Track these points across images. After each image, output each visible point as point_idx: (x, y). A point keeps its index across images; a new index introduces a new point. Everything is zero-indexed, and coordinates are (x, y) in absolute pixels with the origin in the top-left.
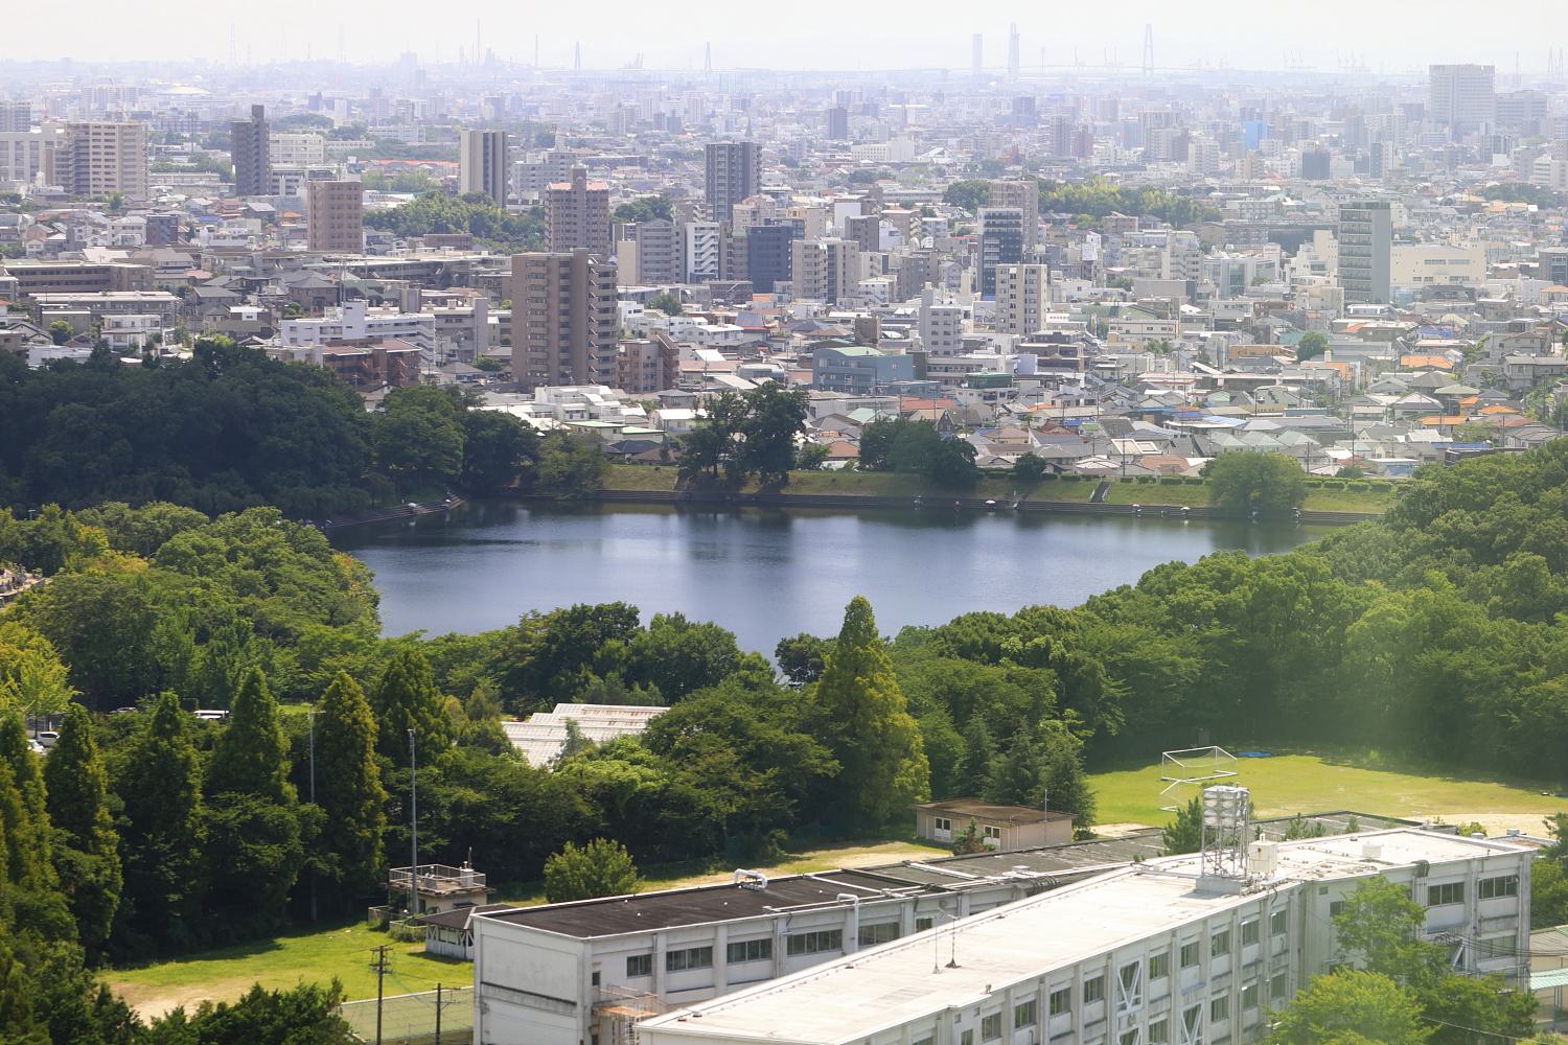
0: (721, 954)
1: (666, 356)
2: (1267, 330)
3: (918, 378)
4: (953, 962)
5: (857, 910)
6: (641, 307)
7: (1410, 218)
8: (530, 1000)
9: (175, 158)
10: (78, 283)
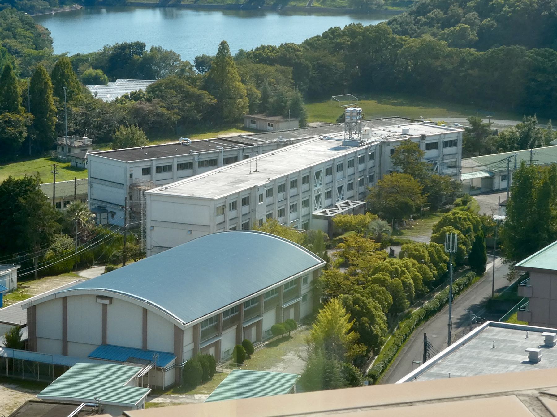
0: (175, 167)
5: (223, 152)
8: (108, 183)
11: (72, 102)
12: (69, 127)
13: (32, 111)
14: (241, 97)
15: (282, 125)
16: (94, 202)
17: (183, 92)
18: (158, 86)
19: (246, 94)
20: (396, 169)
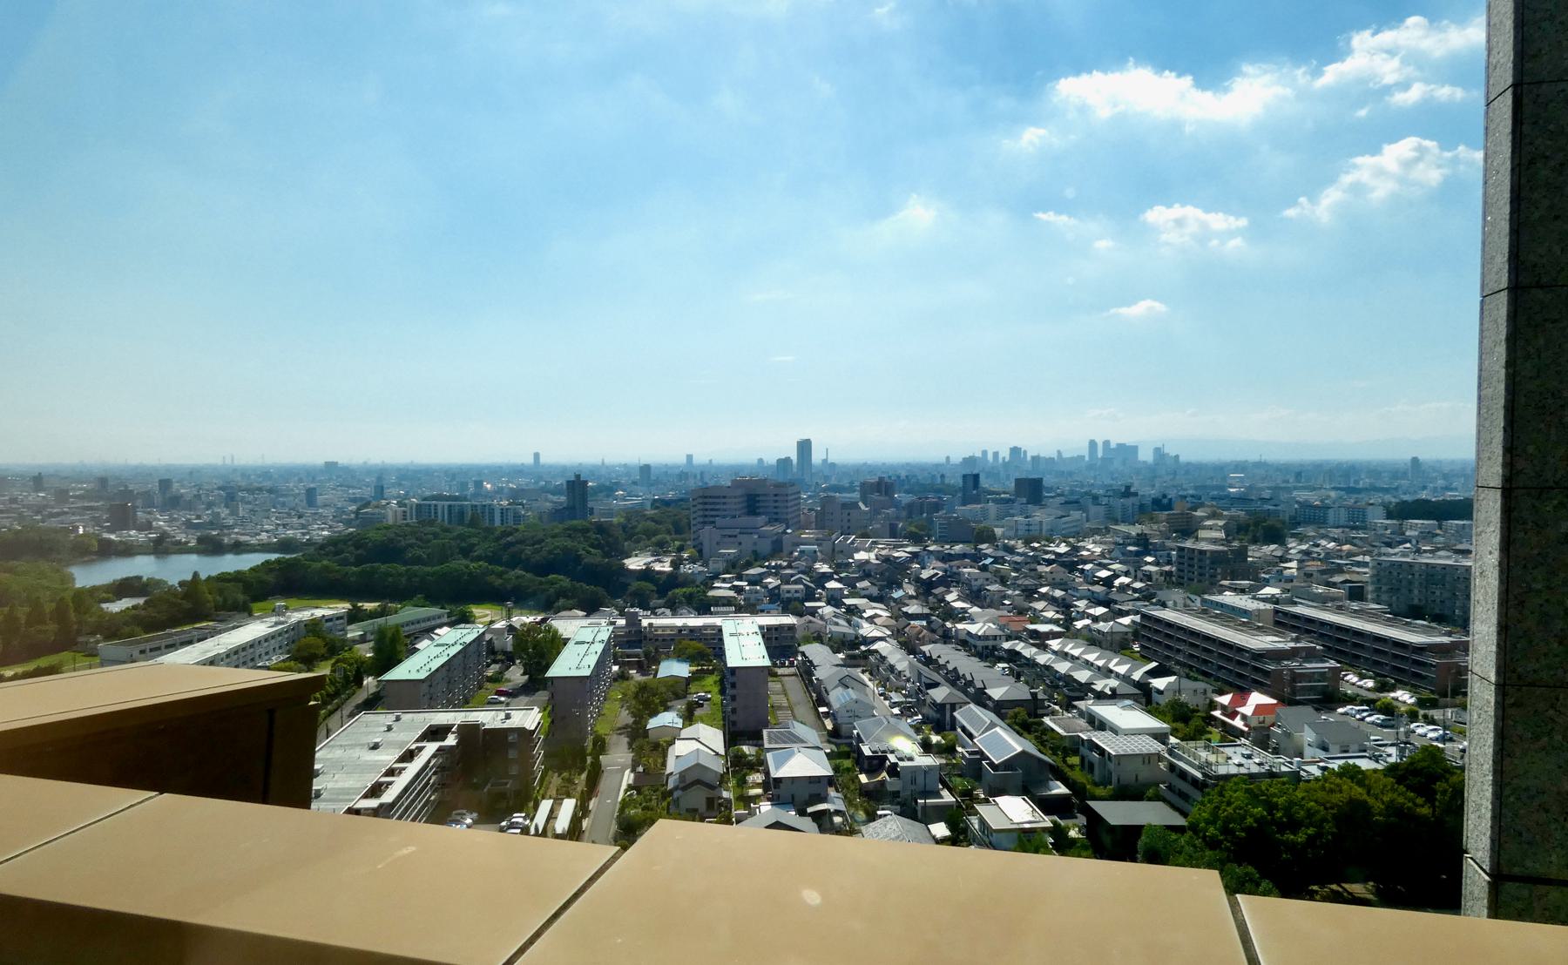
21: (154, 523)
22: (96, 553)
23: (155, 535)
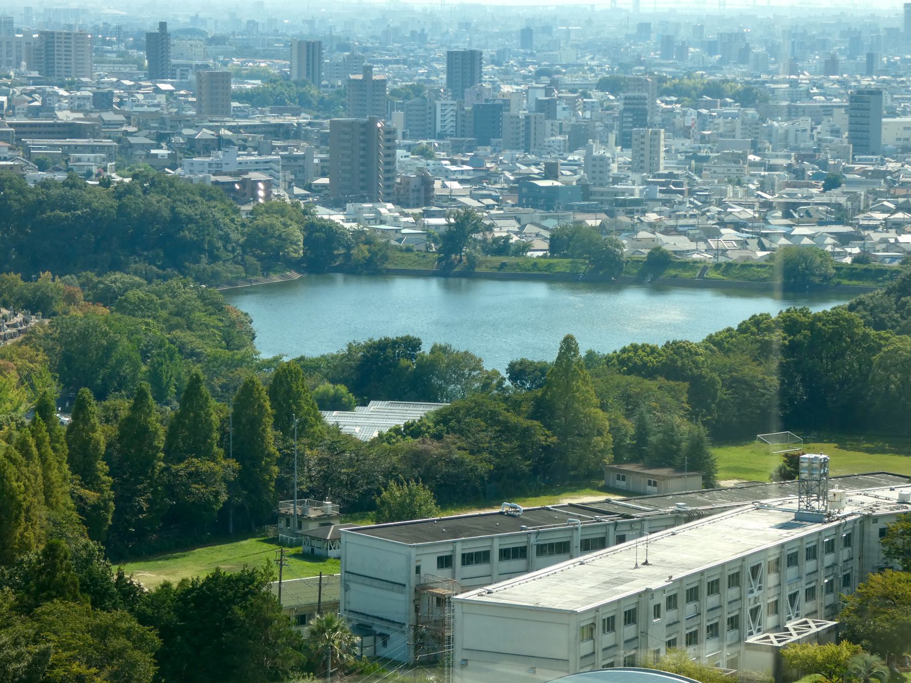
0: (495, 555)
1: (426, 183)
2: (803, 171)
3: (584, 200)
4: (647, 561)
5: (580, 529)
6: (409, 154)
7: (892, 100)
8: (376, 583)
9: (109, 55)
10: (53, 133)
11: (304, 440)
12: (299, 484)
13: (237, 456)
14: (600, 434)
15: (674, 484)
16: (352, 616)
17: (498, 422)
18: (454, 412)
19: (608, 428)
20: (890, 565)
21: (437, 184)
22: (295, 265)
23: (442, 221)
